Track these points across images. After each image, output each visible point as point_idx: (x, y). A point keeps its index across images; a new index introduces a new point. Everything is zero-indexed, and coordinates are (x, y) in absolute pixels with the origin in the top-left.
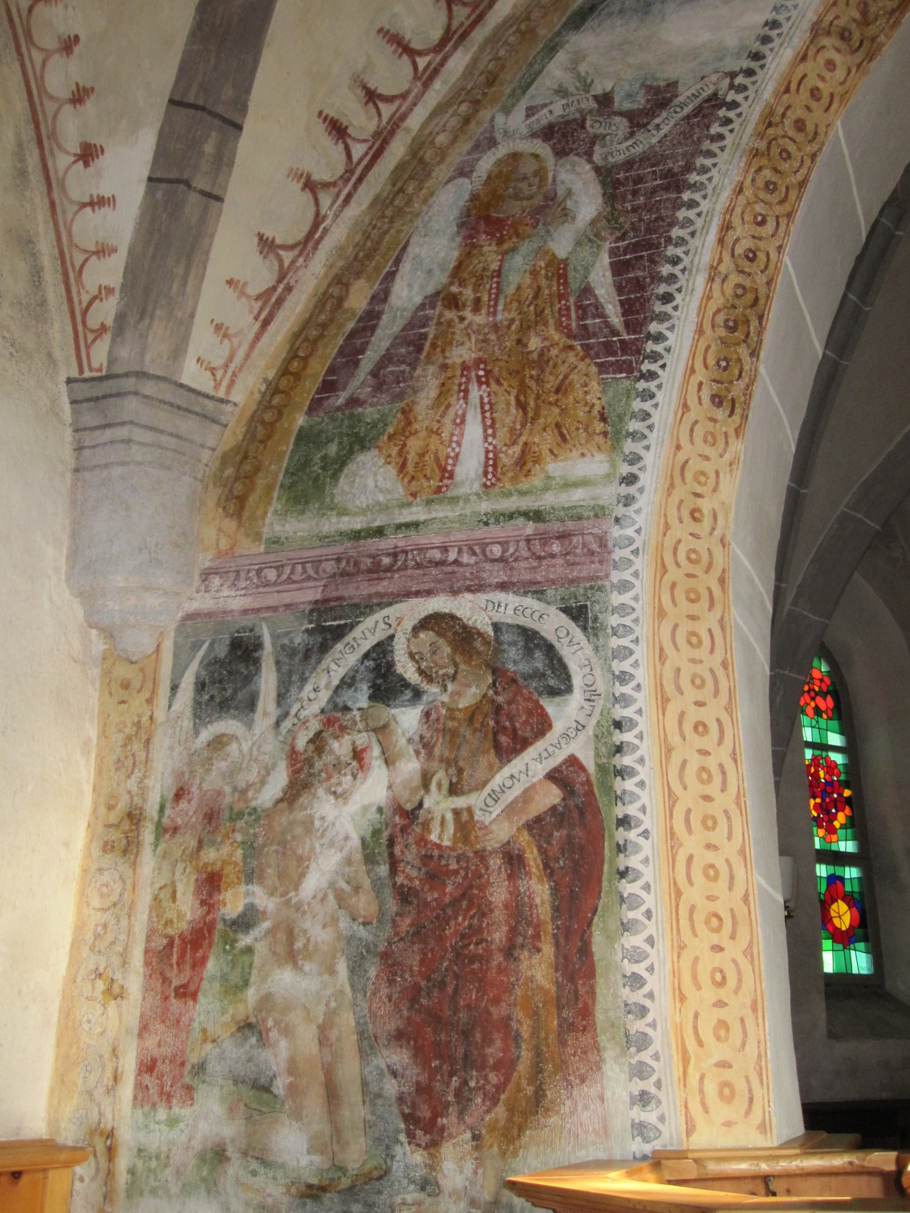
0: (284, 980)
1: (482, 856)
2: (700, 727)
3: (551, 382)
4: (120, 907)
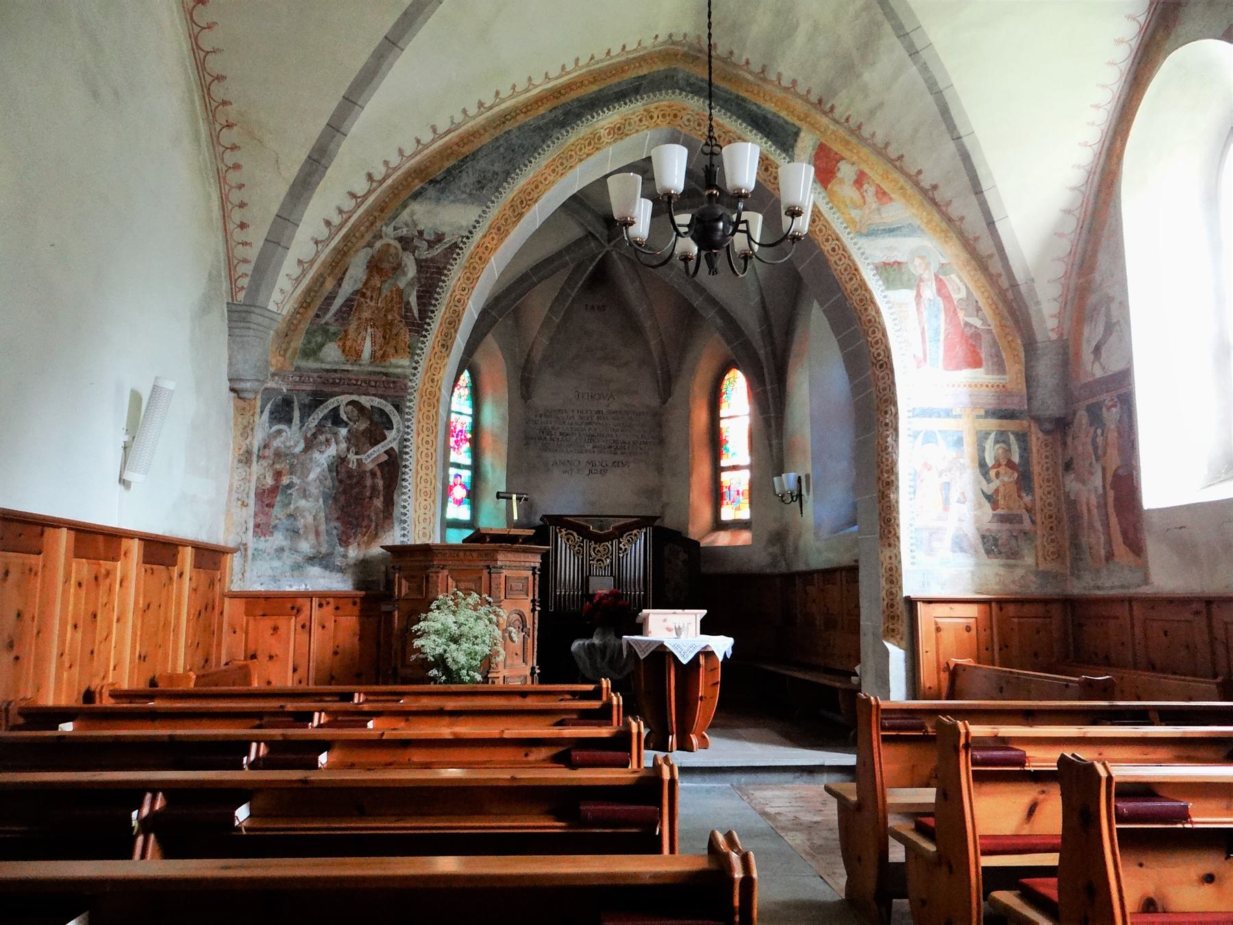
0: (302, 503)
1: (365, 472)
2: (427, 442)
3: (394, 332)
4: (246, 480)
